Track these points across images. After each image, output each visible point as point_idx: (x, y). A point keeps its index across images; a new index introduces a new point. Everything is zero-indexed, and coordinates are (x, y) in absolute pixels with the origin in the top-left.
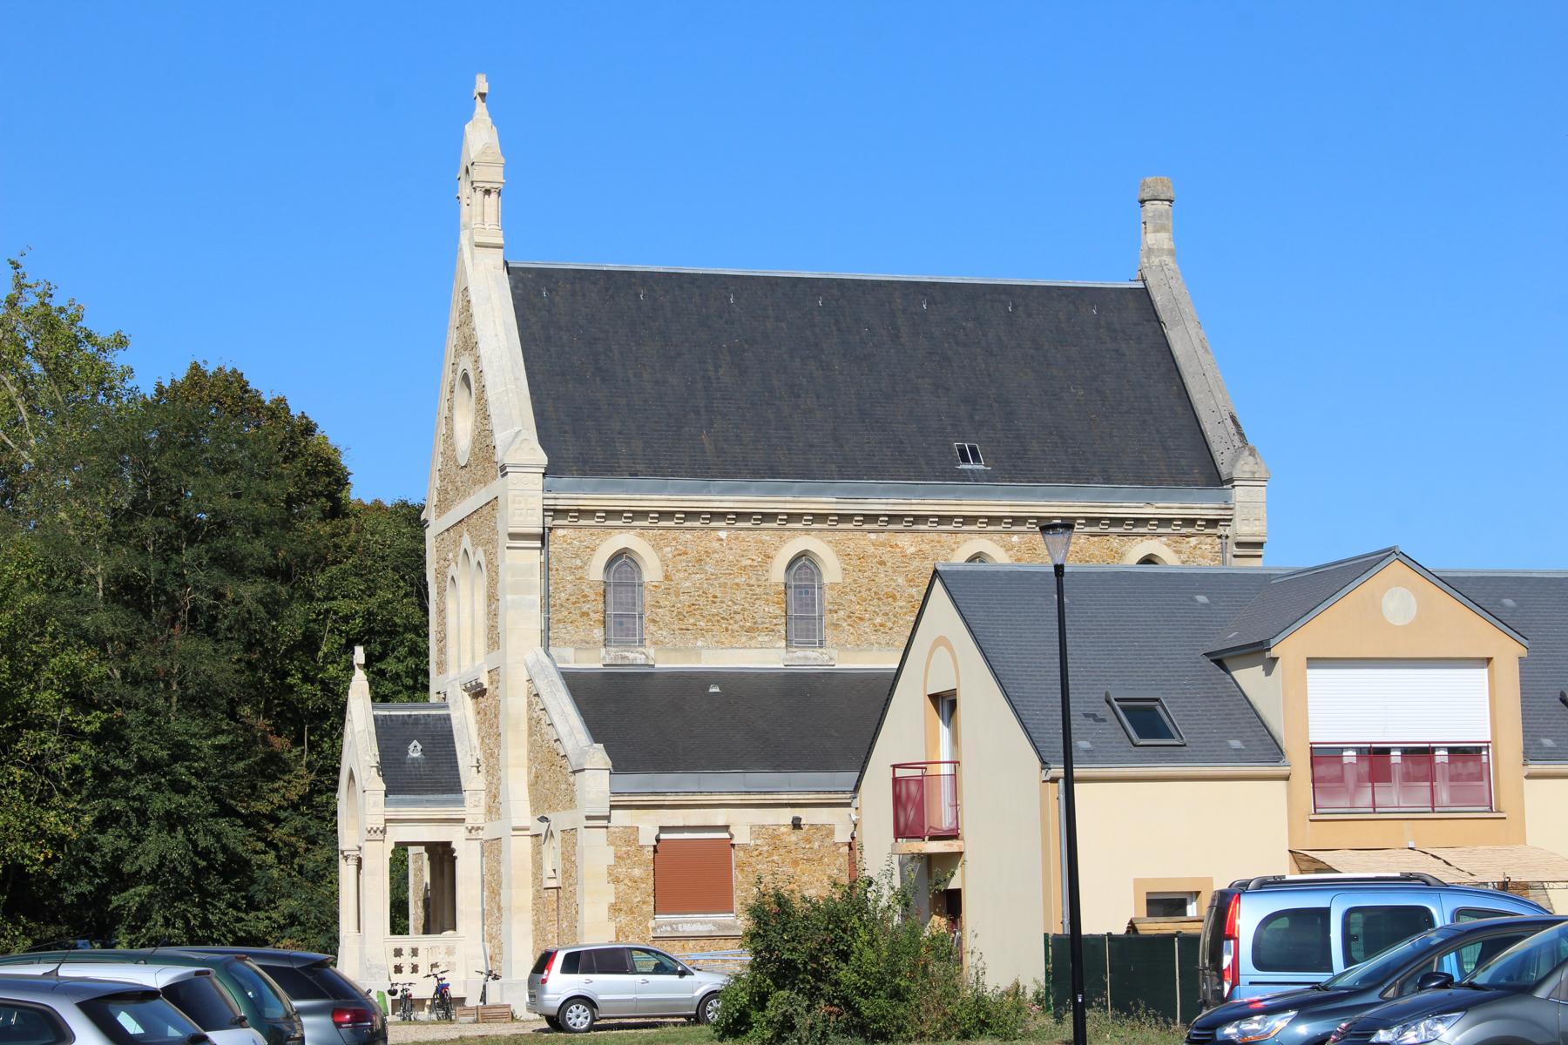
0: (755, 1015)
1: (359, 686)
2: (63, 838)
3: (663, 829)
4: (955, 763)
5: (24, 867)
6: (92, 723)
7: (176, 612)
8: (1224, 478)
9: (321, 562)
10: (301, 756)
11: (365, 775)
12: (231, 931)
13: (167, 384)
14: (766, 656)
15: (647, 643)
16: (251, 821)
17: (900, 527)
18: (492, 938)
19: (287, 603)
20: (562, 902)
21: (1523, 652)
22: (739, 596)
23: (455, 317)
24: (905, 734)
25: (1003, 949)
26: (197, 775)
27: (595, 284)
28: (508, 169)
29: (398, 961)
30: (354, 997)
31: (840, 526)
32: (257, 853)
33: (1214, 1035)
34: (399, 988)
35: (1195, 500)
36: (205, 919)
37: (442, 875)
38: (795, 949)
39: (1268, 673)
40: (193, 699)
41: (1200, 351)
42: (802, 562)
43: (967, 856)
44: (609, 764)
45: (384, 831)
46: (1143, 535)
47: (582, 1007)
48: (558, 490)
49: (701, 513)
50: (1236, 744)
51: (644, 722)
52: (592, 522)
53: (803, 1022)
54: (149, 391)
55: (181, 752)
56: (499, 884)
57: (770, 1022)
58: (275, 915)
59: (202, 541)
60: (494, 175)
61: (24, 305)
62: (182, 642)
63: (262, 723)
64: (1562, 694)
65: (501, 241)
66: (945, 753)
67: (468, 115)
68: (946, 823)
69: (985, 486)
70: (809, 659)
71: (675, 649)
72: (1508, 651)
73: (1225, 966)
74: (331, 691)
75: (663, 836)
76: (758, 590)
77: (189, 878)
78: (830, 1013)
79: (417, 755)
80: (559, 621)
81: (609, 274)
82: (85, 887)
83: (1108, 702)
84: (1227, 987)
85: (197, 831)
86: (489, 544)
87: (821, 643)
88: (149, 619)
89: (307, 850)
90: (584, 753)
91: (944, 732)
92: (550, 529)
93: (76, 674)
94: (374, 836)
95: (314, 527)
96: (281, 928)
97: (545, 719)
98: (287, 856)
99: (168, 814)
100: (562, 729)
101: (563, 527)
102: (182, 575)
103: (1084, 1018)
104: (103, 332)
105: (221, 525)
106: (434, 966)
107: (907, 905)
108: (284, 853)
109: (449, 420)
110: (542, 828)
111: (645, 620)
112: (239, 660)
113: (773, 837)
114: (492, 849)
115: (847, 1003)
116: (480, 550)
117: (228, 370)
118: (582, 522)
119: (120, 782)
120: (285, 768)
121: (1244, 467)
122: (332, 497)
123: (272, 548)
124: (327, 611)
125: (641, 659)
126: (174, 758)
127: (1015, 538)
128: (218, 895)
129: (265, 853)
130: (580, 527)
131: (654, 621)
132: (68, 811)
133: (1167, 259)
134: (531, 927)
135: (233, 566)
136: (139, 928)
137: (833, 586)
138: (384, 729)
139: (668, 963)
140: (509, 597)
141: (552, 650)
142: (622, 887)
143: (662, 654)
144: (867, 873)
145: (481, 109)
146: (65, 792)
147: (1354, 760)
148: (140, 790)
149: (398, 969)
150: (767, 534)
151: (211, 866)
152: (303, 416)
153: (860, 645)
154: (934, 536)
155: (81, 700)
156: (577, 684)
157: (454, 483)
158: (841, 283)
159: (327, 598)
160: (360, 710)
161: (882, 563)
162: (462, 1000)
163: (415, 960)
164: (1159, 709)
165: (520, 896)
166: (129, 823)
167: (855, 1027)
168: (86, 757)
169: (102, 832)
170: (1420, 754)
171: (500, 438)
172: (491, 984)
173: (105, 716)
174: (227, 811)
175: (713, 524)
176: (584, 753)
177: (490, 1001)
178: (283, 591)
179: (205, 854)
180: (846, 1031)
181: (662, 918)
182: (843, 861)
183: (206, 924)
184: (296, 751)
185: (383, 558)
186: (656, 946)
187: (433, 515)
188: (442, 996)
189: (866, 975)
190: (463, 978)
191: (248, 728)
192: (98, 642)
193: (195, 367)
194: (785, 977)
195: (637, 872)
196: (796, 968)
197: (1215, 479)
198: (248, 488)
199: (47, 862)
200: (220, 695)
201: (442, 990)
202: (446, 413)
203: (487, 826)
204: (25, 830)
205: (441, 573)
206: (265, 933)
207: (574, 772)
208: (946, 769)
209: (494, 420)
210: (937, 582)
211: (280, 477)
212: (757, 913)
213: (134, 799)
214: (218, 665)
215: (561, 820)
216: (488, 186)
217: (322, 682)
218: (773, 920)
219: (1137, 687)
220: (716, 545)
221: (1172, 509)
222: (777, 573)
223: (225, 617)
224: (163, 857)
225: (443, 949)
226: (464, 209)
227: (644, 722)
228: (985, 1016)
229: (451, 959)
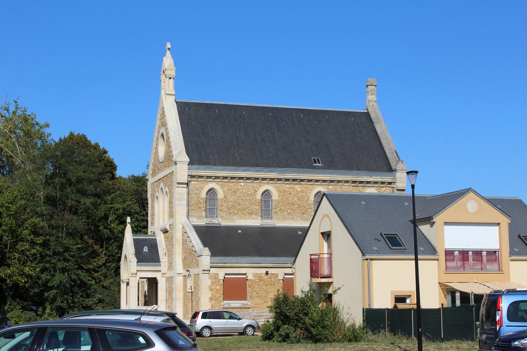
0: (275, 333)
1: (128, 229)
3: (226, 274)
6: (40, 240)
7: (65, 207)
8: (393, 170)
9: (109, 193)
10: (103, 251)
11: (130, 257)
12: (81, 304)
13: (63, 138)
15: (219, 217)
16: (88, 271)
22: (247, 203)
23: (159, 117)
24: (312, 245)
25: (351, 313)
28: (176, 72)
33: (511, 345)
40: (70, 233)
41: (385, 131)
42: (267, 193)
44: (210, 254)
45: (136, 274)
46: (369, 187)
49: (235, 177)
51: (221, 241)
54: (57, 140)
55: (67, 249)
56: (172, 291)
59: (74, 186)
60: (172, 73)
61: (18, 114)
62: (67, 216)
63: (91, 241)
65: (174, 93)
66: (326, 250)
67: (164, 55)
68: (326, 272)
69: (322, 171)
71: (227, 219)
72: (505, 221)
74: (112, 232)
75: (226, 276)
76: (253, 201)
78: (301, 333)
80: (192, 210)
81: (207, 104)
82: (36, 290)
83: (381, 235)
84: (498, 328)
86: (170, 186)
88: (57, 209)
89: (104, 280)
90: (202, 251)
91: (325, 245)
95: (107, 182)
96: (96, 304)
97: (188, 240)
98: (98, 281)
99: (63, 268)
101: (193, 181)
102: (67, 196)
104: (42, 122)
105: (79, 181)
108: (97, 281)
109: (157, 148)
110: (187, 273)
112: (85, 222)
113: (260, 277)
114: (170, 280)
115: (307, 329)
117: (81, 134)
118: (199, 179)
119: (48, 258)
122: (112, 173)
124: (111, 208)
125: (217, 222)
127: (331, 187)
128: (77, 293)
129: (92, 280)
130: (199, 181)
132: (32, 267)
133: (375, 104)
134: (182, 304)
135: (83, 193)
136: (53, 303)
138: (136, 242)
140: (177, 202)
143: (223, 220)
145: (168, 53)
146: (32, 262)
148: (54, 261)
150: (256, 184)
152: (104, 149)
153: (284, 218)
154: (306, 186)
155: (36, 233)
156: (198, 229)
157: (159, 165)
160: (129, 237)
161: (291, 194)
164: (397, 237)
165: (179, 294)
166: (50, 271)
168: (38, 250)
169: (42, 274)
170: (478, 253)
171: (175, 153)
173: (44, 238)
174: (81, 268)
175: (239, 181)
176: (202, 251)
178: (99, 201)
179: (74, 281)
181: (225, 302)
183: (73, 302)
184: (101, 250)
186: (230, 310)
187: (150, 177)
192: (42, 215)
195: (218, 287)
196: (290, 318)
197: (390, 170)
199: (25, 283)
202: (155, 146)
203: (168, 273)
207: (199, 256)
208: (326, 256)
209: (173, 148)
210: (325, 197)
211: (97, 166)
213: (52, 263)
214: (79, 223)
216: (170, 76)
217: (110, 229)
220: (240, 187)
221: (378, 179)
222: (259, 196)
223: (81, 209)
224: (61, 282)
226: (163, 84)
227: (221, 241)
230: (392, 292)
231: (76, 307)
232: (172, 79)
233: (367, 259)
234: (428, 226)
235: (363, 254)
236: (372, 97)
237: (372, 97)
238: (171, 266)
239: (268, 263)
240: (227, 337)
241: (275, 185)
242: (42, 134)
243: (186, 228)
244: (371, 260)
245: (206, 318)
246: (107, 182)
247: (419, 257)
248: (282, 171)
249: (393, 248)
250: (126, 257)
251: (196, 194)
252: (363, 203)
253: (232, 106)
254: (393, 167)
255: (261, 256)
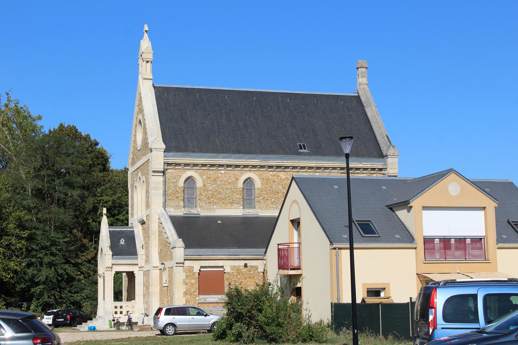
0: (228, 332)
1: (105, 221)
2: (16, 270)
3: (201, 267)
4: (299, 243)
5: (2, 279)
6: (25, 234)
8: (384, 155)
9: (99, 185)
12: (69, 300)
13: (52, 130)
14: (237, 211)
15: (198, 207)
16: (76, 265)
17: (280, 170)
18: (147, 303)
19: (87, 197)
20: (169, 291)
21: (496, 205)
22: (228, 192)
23: (137, 103)
24: (282, 234)
25: (316, 308)
26: (59, 251)
27: (182, 92)
29: (116, 310)
30: (44, 332)
31: (261, 169)
32: (78, 275)
34: (116, 319)
35: (375, 162)
36: (61, 296)
37: (131, 282)
38: (242, 308)
39: (409, 212)
40: (57, 227)
41: (376, 115)
43: (303, 276)
45: (112, 268)
47: (171, 327)
48: (169, 157)
50: (398, 236)
51: (196, 232)
52: (180, 167)
53: (245, 334)
54: (47, 132)
55: (54, 243)
56: (149, 285)
57: (233, 334)
58: (83, 295)
59: (62, 178)
60: (149, 56)
62: (54, 208)
63: (80, 234)
64: (508, 220)
65: (152, 78)
66: (296, 240)
67: (142, 37)
68: (296, 264)
70: (250, 212)
71: (207, 209)
72: (491, 205)
73: (430, 320)
75: (201, 269)
76: (234, 190)
77: (56, 283)
78: (255, 331)
79: (123, 243)
80: (169, 199)
82: (23, 286)
84: (431, 330)
85: (58, 268)
86: (146, 175)
87: (254, 207)
89: (94, 274)
91: (295, 233)
92: (166, 169)
93: (20, 219)
94: (108, 269)
95: (97, 174)
96: (85, 299)
99: (49, 263)
100: (169, 234)
102: (55, 188)
103: (357, 339)
104: (34, 114)
106: (128, 312)
107: (283, 292)
109: (135, 136)
111: (197, 199)
114: (147, 274)
115: (261, 328)
116: (144, 177)
117: (71, 125)
118: (176, 167)
119: (34, 253)
120: (87, 249)
121: (391, 151)
123: (83, 180)
124: (101, 200)
125: (196, 212)
126: (52, 245)
128: (65, 289)
129: (80, 275)
130: (176, 169)
131: (200, 200)
135: (71, 185)
137: (258, 189)
139: (201, 312)
141: (166, 209)
142: (188, 286)
144: (269, 281)
145: (146, 35)
147: (438, 242)
148: (41, 255)
149: (116, 313)
151: (63, 279)
152: (95, 140)
153: (267, 208)
155: (21, 226)
156: (174, 220)
158: (261, 93)
159: (100, 196)
161: (274, 182)
162: (136, 323)
163: (121, 310)
164: (371, 224)
165: (155, 289)
166: (37, 266)
167: (264, 336)
168: (24, 245)
169: (29, 268)
170: (461, 241)
171: (150, 140)
172: (146, 318)
173: (29, 232)
174: (67, 262)
175: (219, 168)
176: (176, 242)
177: (145, 323)
178: (86, 193)
179: (61, 275)
180: (261, 338)
182: (261, 278)
183: (61, 298)
184: (90, 244)
185: (119, 184)
186: (196, 306)
188: (130, 322)
189: (268, 318)
190: (137, 315)
191: (75, 236)
192: (29, 210)
193: (61, 124)
194: (239, 318)
195: (193, 281)
197: (381, 155)
198: (76, 161)
199: (11, 278)
200: (66, 226)
201: (130, 320)
204: (4, 268)
205: (132, 185)
206: (80, 301)
207: (172, 248)
208: (296, 245)
211: (86, 158)
212: (229, 295)
214: (66, 216)
215: (168, 264)
216: (148, 60)
218: (235, 298)
219: (364, 218)
220: (220, 175)
222: (240, 185)
224: (47, 277)
225: (131, 306)
226: (140, 68)
227: (196, 232)
228: (311, 334)
229: (133, 309)
230: (389, 284)
231: (65, 303)
232: (150, 63)
233: (335, 249)
234: (405, 211)
235: (331, 243)
236: (362, 80)
237: (362, 80)
238: (147, 260)
239: (191, 255)
240: (193, 335)
241: (257, 173)
242: (35, 126)
243: (161, 219)
244: (340, 249)
245: (169, 315)
246: (97, 174)
247: (355, 246)
248: (265, 158)
249: (365, 235)
250: (102, 250)
251: (173, 183)
252: (336, 187)
253: (214, 91)
254: (384, 153)
255: (239, 247)
